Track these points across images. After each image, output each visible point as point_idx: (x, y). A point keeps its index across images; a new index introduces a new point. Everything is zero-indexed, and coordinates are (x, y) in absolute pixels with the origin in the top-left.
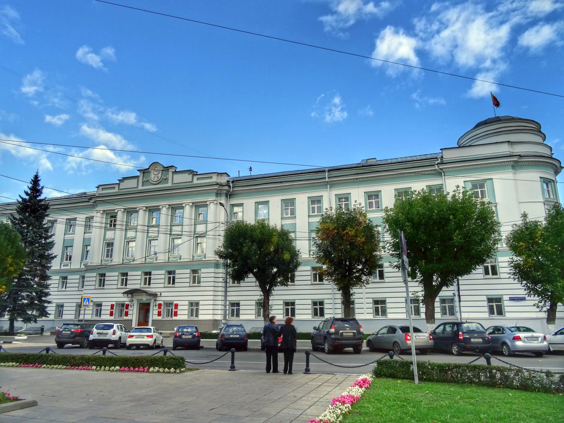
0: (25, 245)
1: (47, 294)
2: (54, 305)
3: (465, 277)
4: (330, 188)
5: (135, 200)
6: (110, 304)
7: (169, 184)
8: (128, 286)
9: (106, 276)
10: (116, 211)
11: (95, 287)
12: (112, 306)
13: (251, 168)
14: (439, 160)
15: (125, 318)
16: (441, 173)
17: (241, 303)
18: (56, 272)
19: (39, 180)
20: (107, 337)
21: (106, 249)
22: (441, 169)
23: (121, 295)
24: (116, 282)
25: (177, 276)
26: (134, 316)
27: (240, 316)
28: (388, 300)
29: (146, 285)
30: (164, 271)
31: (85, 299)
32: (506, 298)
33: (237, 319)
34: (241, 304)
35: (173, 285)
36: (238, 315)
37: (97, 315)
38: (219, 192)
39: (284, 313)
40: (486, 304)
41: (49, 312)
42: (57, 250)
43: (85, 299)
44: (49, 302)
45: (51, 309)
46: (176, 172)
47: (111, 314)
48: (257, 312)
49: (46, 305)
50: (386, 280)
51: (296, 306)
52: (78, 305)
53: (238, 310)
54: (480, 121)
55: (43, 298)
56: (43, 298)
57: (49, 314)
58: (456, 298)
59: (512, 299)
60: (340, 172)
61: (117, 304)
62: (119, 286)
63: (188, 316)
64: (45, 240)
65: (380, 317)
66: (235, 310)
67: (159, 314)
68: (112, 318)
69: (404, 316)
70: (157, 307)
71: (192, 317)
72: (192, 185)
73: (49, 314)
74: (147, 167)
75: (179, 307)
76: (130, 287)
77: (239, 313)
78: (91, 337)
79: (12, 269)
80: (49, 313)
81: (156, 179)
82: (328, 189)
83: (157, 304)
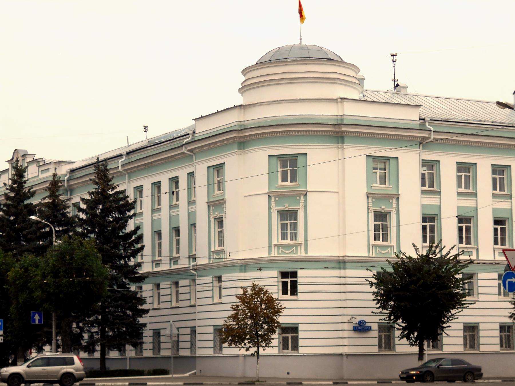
4: (130, 178)
5: (176, 160)
9: (223, 280)
11: (213, 300)
14: (191, 136)
21: (280, 223)
22: (190, 151)
24: (210, 294)
25: (299, 280)
27: (300, 349)
28: (301, 327)
29: (287, 294)
30: (169, 283)
33: (294, 353)
35: (294, 297)
36: (295, 347)
38: (242, 140)
39: (215, 346)
48: (392, 340)
50: (300, 296)
51: (300, 333)
52: (155, 332)
53: (295, 340)
60: (141, 153)
63: (215, 351)
65: (289, 352)
69: (461, 349)
71: (285, 351)
72: (38, 180)
74: (11, 158)
77: (222, 346)
82: (127, 181)
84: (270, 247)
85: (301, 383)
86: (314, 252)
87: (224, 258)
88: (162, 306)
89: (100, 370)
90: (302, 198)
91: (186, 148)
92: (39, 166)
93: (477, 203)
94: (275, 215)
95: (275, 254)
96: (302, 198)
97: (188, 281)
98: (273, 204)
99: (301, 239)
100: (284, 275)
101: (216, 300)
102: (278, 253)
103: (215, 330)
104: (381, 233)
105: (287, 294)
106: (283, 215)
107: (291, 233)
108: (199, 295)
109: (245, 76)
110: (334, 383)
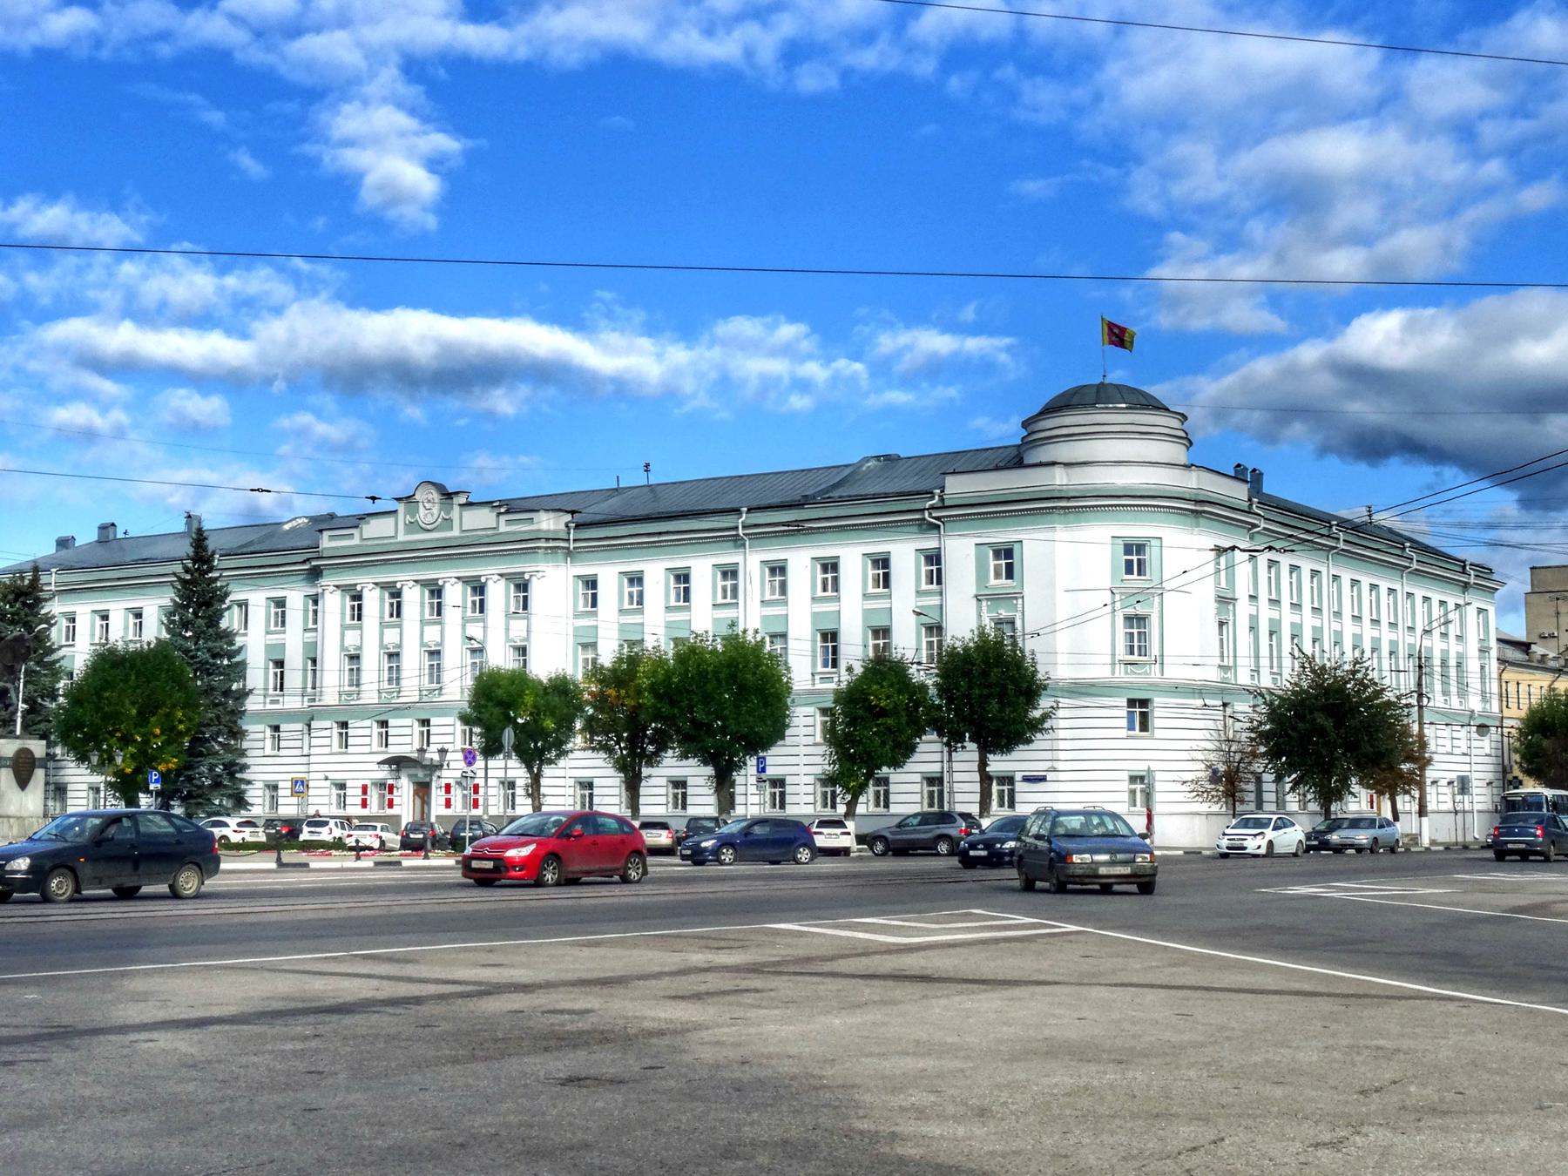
0: (195, 674)
1: (244, 768)
2: (260, 785)
3: (774, 750)
6: (360, 784)
7: (456, 533)
8: (391, 749)
10: (359, 588)
12: (365, 789)
13: (647, 465)
15: (389, 812)
16: (939, 526)
17: (596, 782)
18: (260, 716)
19: (206, 539)
20: (321, 837)
22: (937, 518)
23: (376, 767)
26: (405, 807)
31: (297, 782)
32: (1018, 777)
34: (787, 782)
37: (677, 805)
40: (1126, 786)
41: (250, 800)
42: (257, 675)
43: (297, 782)
44: (249, 782)
45: (256, 796)
46: (469, 504)
47: (364, 804)
49: (243, 787)
54: (1057, 393)
55: (238, 775)
56: (238, 775)
57: (252, 805)
58: (946, 775)
59: (1027, 779)
61: (373, 784)
62: (375, 748)
64: (229, 660)
66: (1006, 792)
67: (448, 804)
68: (365, 812)
70: (443, 789)
73: (252, 805)
75: (360, 802)
76: (394, 751)
78: (302, 837)
79: (181, 727)
80: (738, 778)
81: (430, 519)
83: (443, 785)
84: (1113, 664)
85: (1200, 853)
86: (1176, 672)
87: (337, 689)
88: (282, 752)
89: (1079, 827)
90: (1157, 599)
91: (930, 514)
92: (499, 514)
93: (507, 630)
94: (1120, 620)
95: (1121, 675)
96: (1157, 599)
97: (329, 722)
98: (984, 609)
99: (1155, 651)
100: (1132, 703)
101: (268, 751)
102: (1126, 673)
103: (816, 779)
104: (1136, 644)
105: (1134, 729)
106: (1129, 619)
107: (1140, 647)
108: (1211, 724)
109: (1026, 429)
110: (1185, 853)
